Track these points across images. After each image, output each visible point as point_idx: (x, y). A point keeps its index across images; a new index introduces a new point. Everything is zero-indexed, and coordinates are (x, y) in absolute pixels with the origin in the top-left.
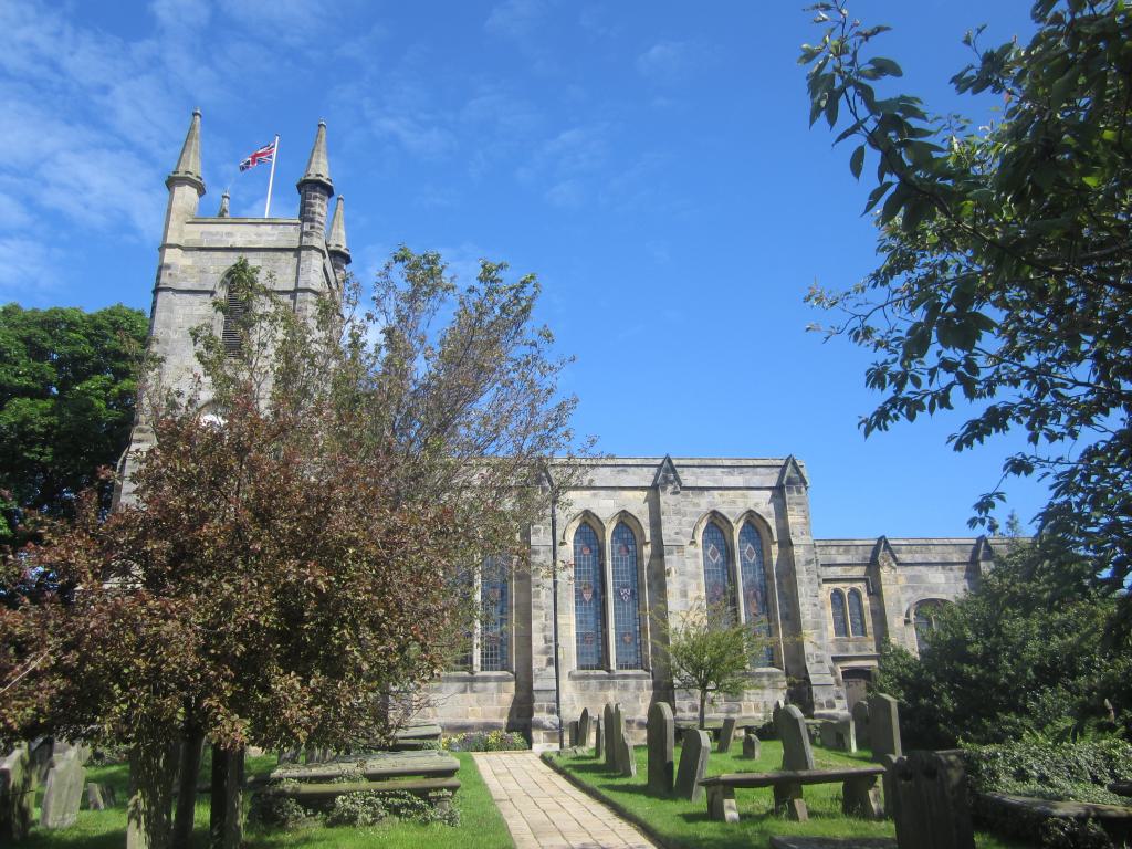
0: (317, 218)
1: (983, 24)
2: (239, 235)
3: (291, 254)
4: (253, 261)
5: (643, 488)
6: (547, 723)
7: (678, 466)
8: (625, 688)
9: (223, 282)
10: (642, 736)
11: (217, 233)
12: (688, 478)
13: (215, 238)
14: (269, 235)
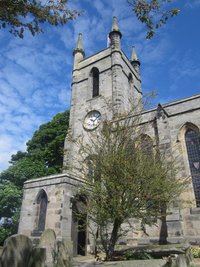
0: (116, 42)
3: (109, 57)
4: (96, 65)
7: (164, 107)
9: (90, 75)
10: (63, 265)
11: (87, 62)
12: (171, 110)
13: (87, 63)
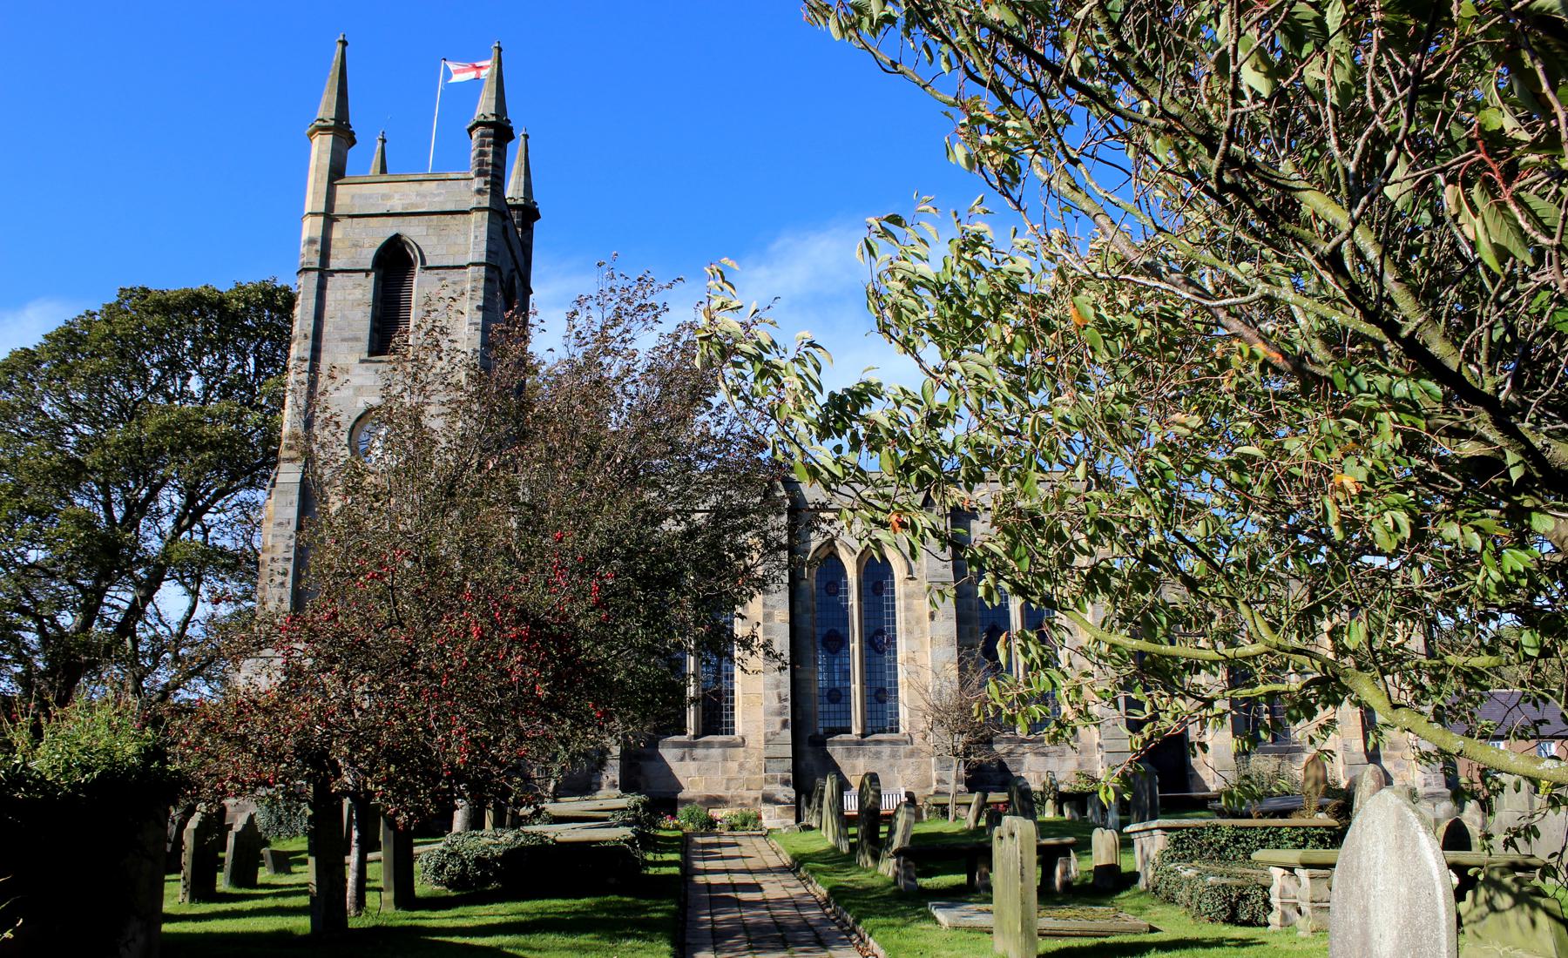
1: (1264, 939)
2: (397, 196)
4: (413, 231)
5: (372, 862)
6: (781, 797)
8: (878, 755)
11: (371, 196)
14: (435, 195)
